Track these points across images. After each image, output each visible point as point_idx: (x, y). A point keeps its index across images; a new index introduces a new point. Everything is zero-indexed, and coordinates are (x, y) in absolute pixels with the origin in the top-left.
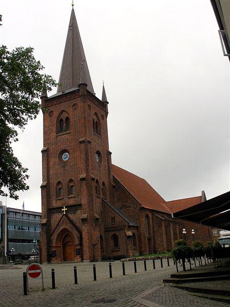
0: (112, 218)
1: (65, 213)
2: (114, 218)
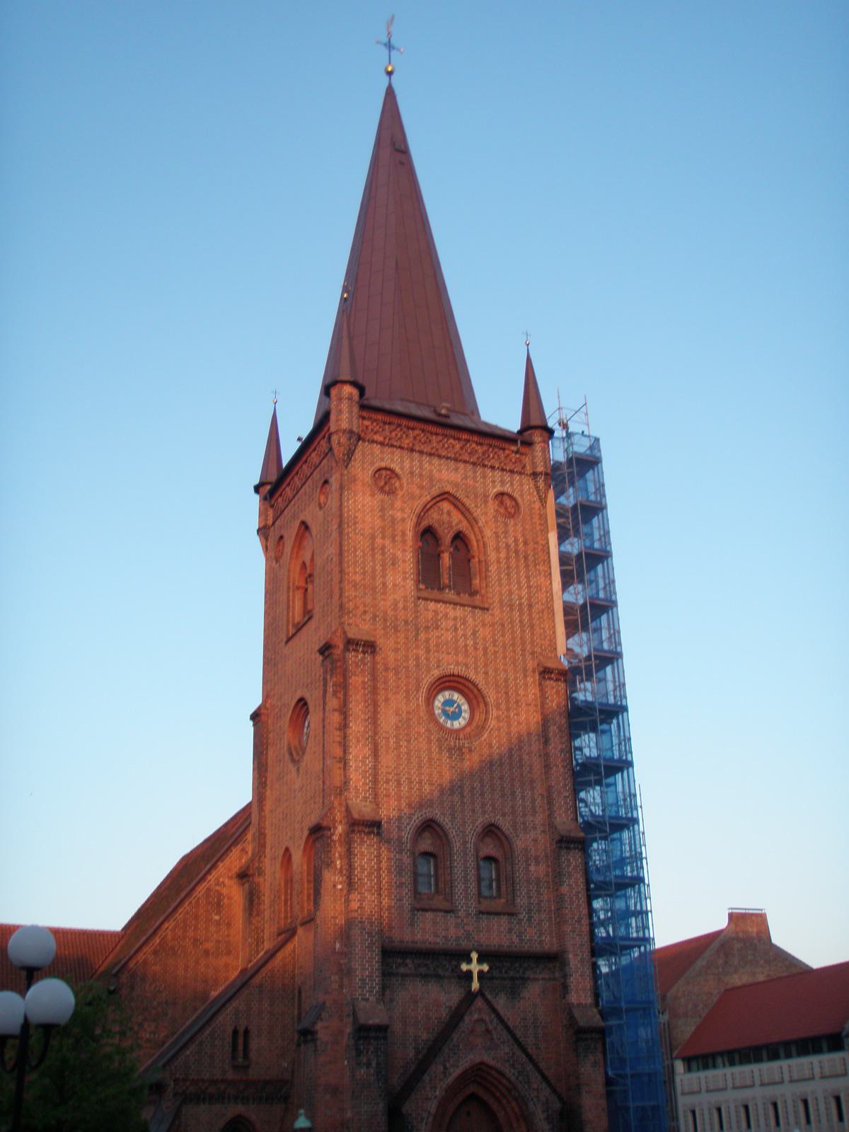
0: (235, 1032)
1: (475, 985)
2: (247, 1032)
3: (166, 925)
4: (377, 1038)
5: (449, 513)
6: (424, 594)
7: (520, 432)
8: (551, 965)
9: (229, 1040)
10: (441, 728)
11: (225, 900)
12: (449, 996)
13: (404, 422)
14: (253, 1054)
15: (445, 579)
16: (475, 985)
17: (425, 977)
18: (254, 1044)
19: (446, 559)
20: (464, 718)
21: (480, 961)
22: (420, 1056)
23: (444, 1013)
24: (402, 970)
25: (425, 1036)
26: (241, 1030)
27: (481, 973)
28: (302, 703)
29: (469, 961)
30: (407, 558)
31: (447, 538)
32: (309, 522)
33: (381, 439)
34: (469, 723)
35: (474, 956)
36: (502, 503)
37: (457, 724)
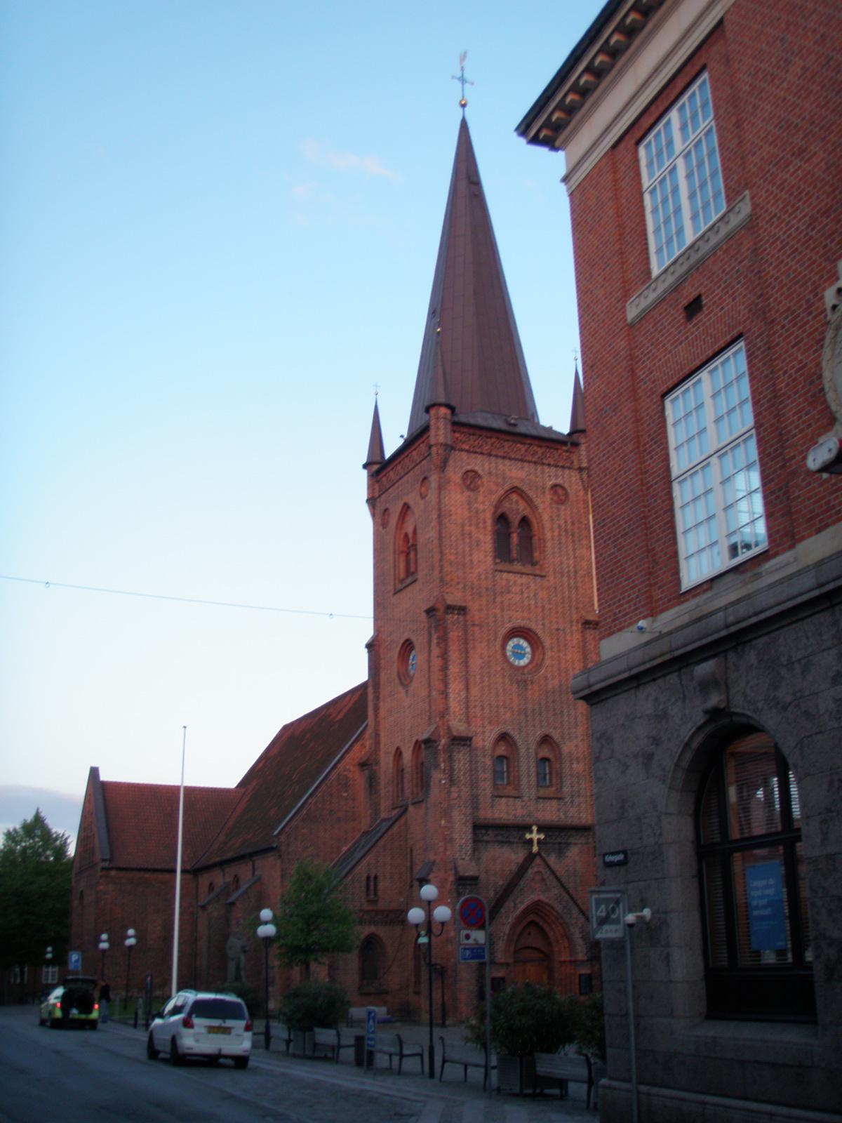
0: (368, 878)
1: (535, 849)
2: (376, 878)
3: (310, 801)
4: (471, 885)
5: (517, 502)
6: (499, 567)
7: (570, 434)
8: (586, 834)
9: (364, 883)
10: (511, 666)
11: (351, 782)
12: (516, 856)
13: (484, 433)
14: (380, 893)
15: (514, 554)
16: (535, 849)
17: (501, 843)
18: (381, 885)
19: (515, 538)
20: (528, 658)
21: (539, 831)
22: (498, 896)
23: (514, 867)
24: (486, 838)
25: (501, 883)
26: (372, 876)
27: (539, 839)
28: (407, 643)
29: (531, 832)
30: (487, 540)
31: (515, 520)
32: (412, 504)
33: (467, 447)
34: (531, 662)
35: (535, 828)
36: (555, 492)
37: (524, 662)
